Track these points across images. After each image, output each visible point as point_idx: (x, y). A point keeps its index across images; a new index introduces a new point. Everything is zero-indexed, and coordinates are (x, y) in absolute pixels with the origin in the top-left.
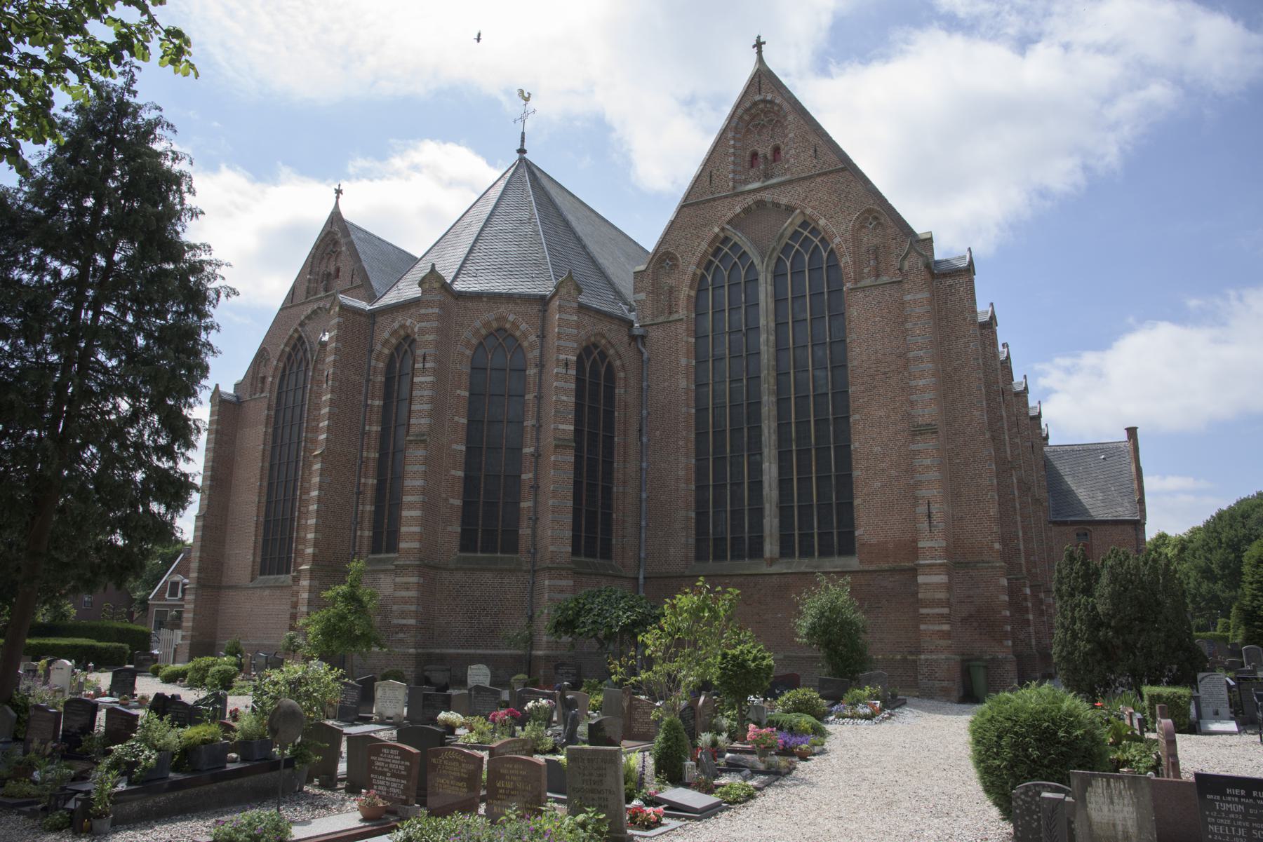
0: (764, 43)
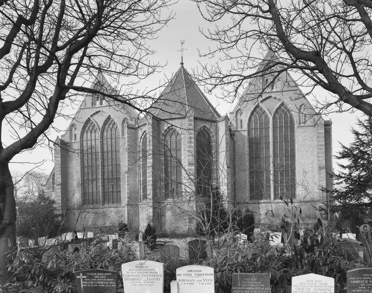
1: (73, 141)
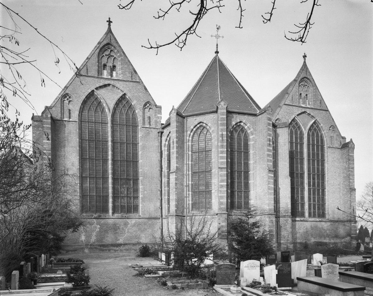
0: (107, 21)
1: (65, 119)
